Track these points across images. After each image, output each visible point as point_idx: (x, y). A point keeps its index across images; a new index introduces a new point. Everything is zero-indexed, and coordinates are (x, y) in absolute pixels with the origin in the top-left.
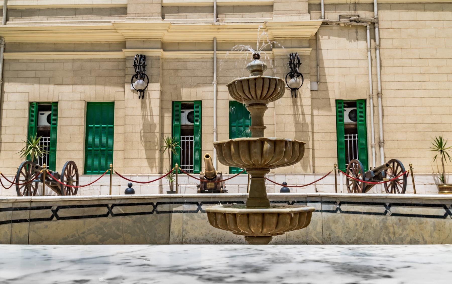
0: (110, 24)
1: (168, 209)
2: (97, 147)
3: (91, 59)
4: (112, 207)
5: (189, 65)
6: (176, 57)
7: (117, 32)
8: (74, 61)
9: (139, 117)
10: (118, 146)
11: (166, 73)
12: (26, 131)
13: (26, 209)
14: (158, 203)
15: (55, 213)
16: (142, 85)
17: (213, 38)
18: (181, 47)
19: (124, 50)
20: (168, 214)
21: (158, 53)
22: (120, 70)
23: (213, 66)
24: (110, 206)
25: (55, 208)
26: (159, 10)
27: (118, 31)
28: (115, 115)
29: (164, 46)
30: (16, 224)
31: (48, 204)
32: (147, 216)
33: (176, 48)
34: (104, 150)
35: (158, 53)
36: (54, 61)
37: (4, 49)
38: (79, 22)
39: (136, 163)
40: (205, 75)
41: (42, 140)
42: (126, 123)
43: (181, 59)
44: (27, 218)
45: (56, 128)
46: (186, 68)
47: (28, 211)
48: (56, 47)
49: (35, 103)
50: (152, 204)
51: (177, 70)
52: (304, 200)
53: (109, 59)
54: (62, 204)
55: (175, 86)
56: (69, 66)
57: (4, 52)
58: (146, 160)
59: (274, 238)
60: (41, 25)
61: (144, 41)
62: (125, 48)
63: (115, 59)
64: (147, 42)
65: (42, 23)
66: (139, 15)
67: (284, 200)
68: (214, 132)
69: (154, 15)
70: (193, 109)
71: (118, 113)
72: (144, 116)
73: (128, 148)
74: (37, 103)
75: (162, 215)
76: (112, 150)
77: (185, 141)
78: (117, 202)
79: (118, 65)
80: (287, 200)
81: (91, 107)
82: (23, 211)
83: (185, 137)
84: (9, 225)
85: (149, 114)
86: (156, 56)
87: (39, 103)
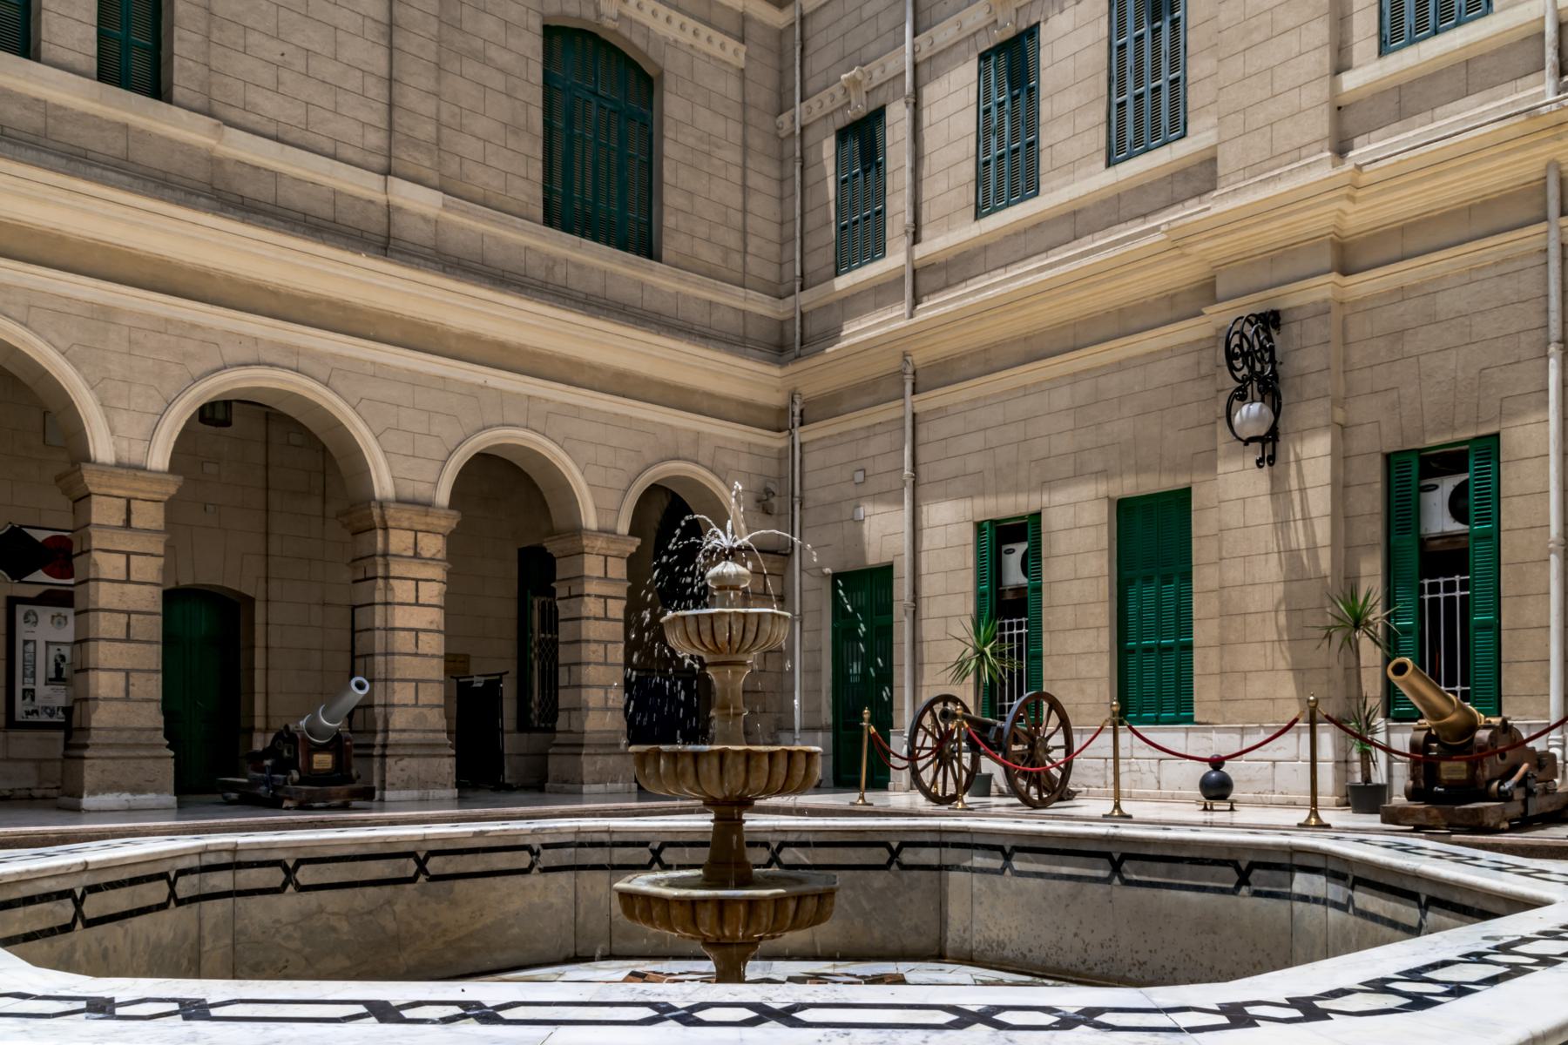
0: (1157, 237)
1: (935, 861)
2: (1149, 638)
3: (1120, 363)
4: (779, 849)
5: (1447, 302)
6: (1397, 284)
7: (1183, 255)
8: (1075, 377)
9: (1271, 530)
10: (1203, 633)
11: (1356, 355)
12: (971, 608)
13: (601, 844)
14: (903, 845)
15: (656, 854)
16: (1259, 418)
17: (1542, 166)
18: (1413, 244)
19: (1207, 310)
20: (934, 873)
21: (1323, 288)
22: (1203, 378)
23: (1546, 284)
24: (775, 846)
25: (656, 846)
26: (1320, 124)
27: (1187, 251)
28: (1195, 530)
29: (1346, 257)
30: (585, 873)
31: (643, 838)
32: (872, 873)
33: (1396, 251)
34: (1169, 648)
35: (1323, 288)
36: (1025, 390)
37: (914, 384)
38: (1040, 270)
39: (1257, 686)
40: (1512, 330)
41: (1002, 627)
42: (1224, 554)
43: (1414, 287)
44: (605, 862)
45: (1038, 589)
46: (1433, 320)
47: (607, 849)
48: (1031, 350)
49: (986, 525)
50: (886, 845)
51: (1399, 334)
52: (1285, 860)
53: (1171, 349)
54: (669, 838)
55: (1394, 395)
56: (1062, 398)
57: (914, 393)
58: (1290, 674)
59: (762, 946)
60: (980, 297)
61: (1272, 259)
62: (1214, 300)
63: (1189, 344)
64: (1284, 260)
65: (994, 285)
66: (1255, 170)
67: (1225, 856)
68: (1550, 551)
69: (1304, 152)
70: (1467, 471)
71: (1202, 524)
72: (1282, 523)
73: (1232, 638)
74: (991, 521)
75: (915, 873)
76: (1189, 647)
77: (1442, 595)
78: (791, 838)
79: (1199, 363)
80: (1234, 857)
81: (1127, 511)
82: (598, 849)
83: (1441, 580)
84: (571, 874)
85: (1299, 516)
86: (1315, 303)
87: (997, 522)
